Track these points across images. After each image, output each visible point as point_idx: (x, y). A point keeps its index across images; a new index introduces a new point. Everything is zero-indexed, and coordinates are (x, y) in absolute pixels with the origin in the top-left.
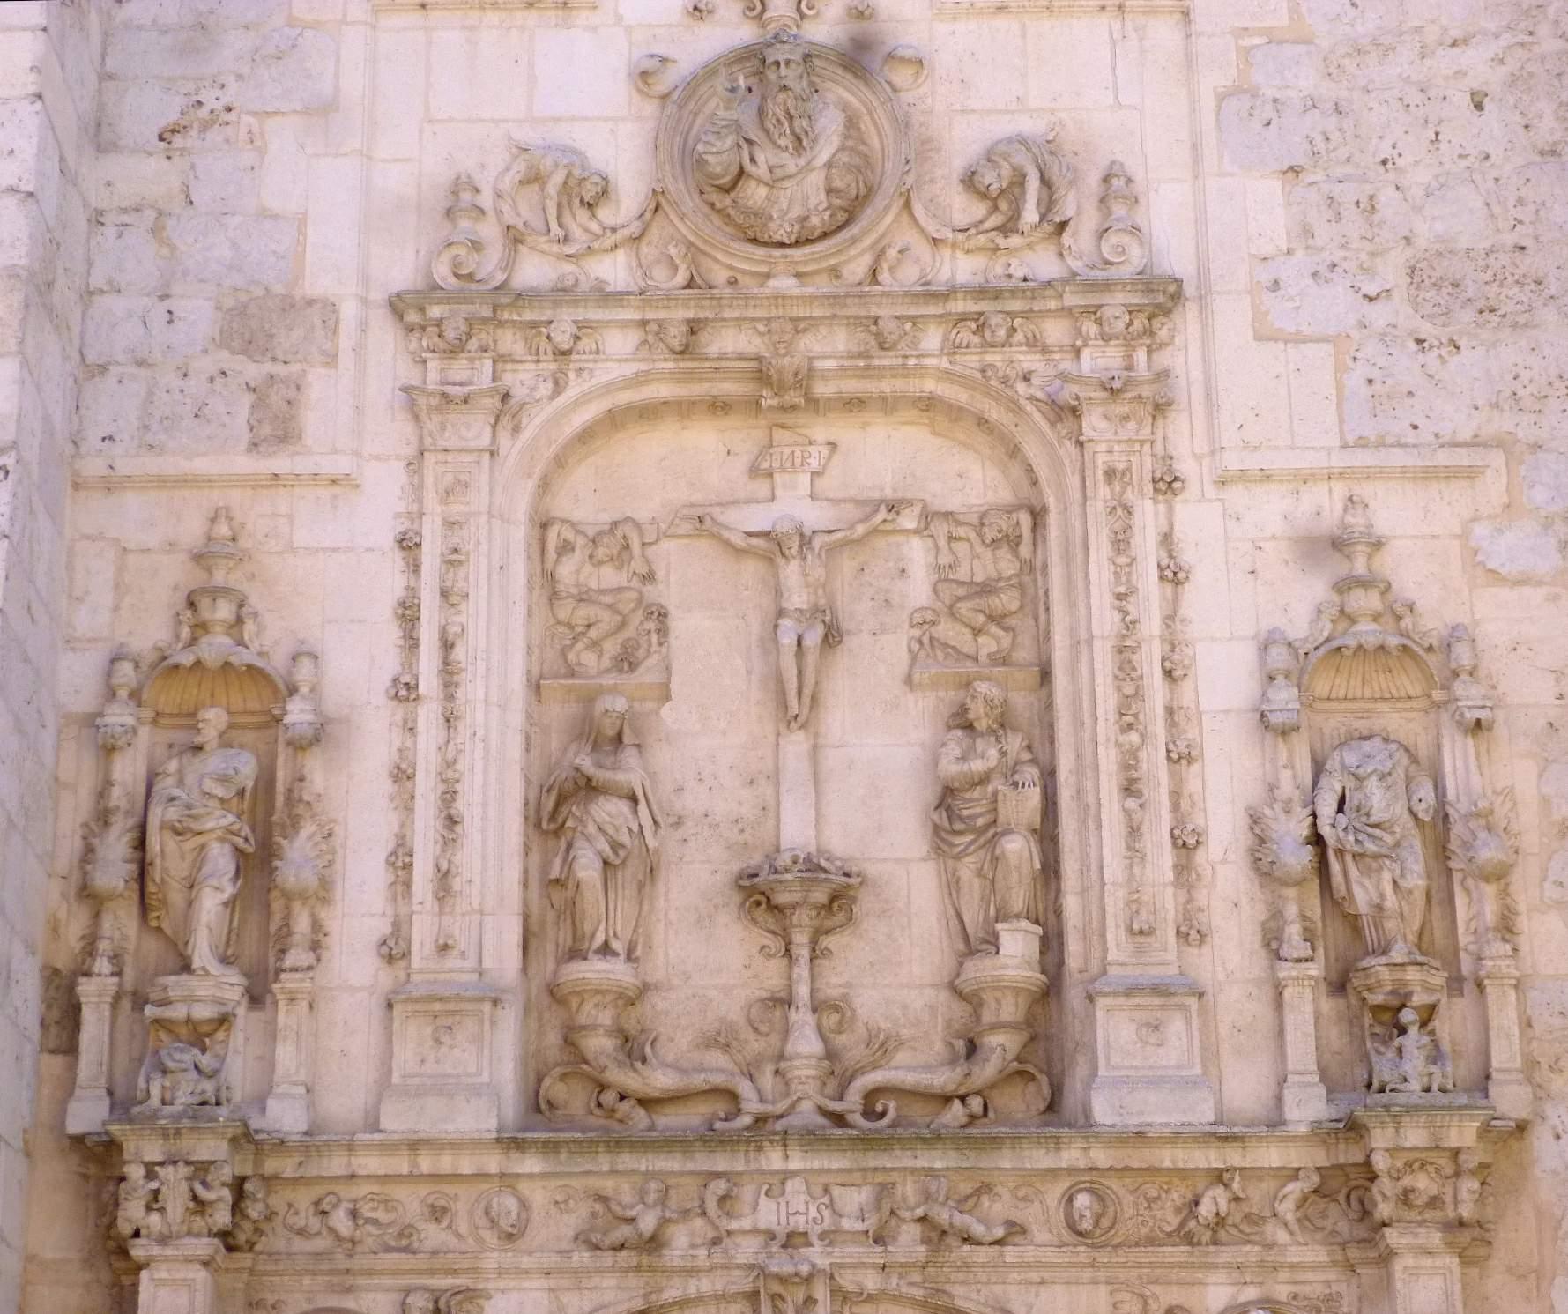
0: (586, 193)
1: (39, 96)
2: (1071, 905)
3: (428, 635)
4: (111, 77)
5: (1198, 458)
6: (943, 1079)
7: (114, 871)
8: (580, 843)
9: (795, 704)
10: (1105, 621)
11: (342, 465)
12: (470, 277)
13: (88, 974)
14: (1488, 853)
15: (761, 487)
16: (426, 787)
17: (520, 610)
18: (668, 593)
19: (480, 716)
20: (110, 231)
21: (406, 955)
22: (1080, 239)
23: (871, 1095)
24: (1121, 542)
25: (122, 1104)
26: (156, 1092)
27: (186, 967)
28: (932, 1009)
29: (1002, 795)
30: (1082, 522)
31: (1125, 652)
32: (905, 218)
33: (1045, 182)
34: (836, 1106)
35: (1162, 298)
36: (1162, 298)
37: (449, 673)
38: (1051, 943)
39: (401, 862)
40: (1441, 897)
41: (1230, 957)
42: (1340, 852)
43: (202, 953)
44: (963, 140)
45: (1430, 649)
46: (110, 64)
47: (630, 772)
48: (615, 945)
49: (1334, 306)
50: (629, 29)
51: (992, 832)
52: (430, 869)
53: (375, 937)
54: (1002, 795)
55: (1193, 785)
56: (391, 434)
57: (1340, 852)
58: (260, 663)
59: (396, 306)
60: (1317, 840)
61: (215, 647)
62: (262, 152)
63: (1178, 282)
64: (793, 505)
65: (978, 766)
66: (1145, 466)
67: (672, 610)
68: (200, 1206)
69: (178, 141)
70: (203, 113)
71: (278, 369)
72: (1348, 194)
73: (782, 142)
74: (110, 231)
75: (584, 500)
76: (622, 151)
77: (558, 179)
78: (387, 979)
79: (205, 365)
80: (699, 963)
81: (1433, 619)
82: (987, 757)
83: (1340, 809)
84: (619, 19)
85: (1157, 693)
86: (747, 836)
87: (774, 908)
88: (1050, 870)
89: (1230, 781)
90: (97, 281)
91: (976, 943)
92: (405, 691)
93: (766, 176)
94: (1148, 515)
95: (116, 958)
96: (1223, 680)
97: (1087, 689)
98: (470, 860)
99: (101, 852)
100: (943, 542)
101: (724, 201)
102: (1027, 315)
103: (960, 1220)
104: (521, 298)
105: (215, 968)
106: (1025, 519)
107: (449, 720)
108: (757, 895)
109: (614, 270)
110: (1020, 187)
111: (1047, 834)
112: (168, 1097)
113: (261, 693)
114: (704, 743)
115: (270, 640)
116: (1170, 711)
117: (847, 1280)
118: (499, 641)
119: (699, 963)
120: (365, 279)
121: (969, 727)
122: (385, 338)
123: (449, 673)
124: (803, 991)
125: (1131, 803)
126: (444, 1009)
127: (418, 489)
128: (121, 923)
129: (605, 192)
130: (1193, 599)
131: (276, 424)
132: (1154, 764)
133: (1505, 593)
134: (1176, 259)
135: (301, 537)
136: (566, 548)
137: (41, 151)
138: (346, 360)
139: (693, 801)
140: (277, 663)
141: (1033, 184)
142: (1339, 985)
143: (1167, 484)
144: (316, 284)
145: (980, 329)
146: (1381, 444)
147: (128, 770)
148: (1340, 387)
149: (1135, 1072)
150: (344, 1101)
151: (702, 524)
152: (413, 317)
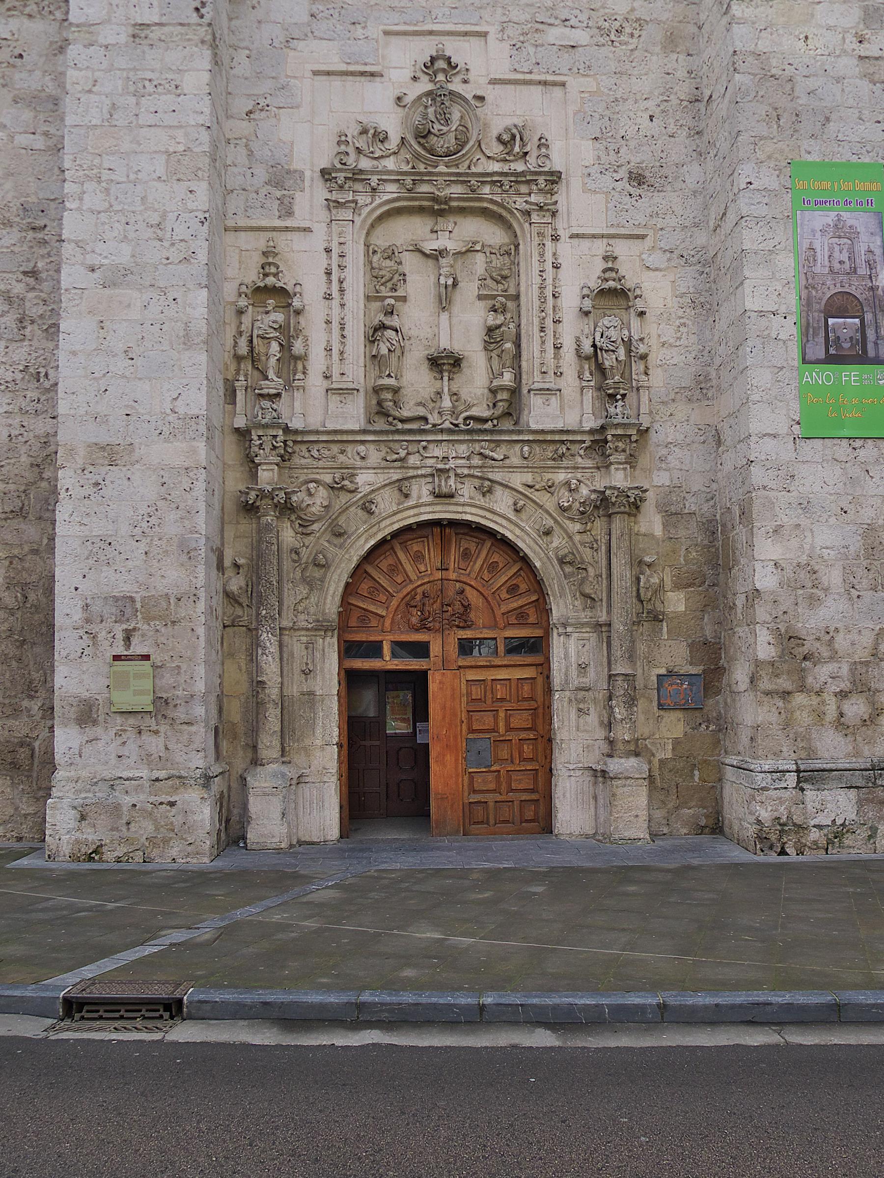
0: (381, 137)
1: (210, 94)
2: (524, 364)
3: (334, 278)
4: (230, 93)
5: (564, 229)
6: (486, 414)
7: (243, 349)
8: (381, 344)
11: (306, 224)
12: (345, 164)
13: (238, 380)
14: (642, 349)
15: (434, 236)
16: (335, 326)
17: (362, 273)
18: (406, 268)
19: (351, 304)
20: (232, 146)
21: (331, 376)
22: (532, 159)
23: (466, 419)
24: (542, 255)
26: (260, 415)
27: (267, 378)
28: (483, 395)
30: (529, 247)
32: (479, 149)
33: (521, 139)
34: (456, 422)
36: (555, 178)
37: (342, 291)
40: (628, 364)
41: (569, 382)
42: (601, 350)
43: (271, 374)
44: (497, 126)
45: (629, 290)
46: (230, 90)
47: (394, 321)
48: (392, 374)
50: (393, 83)
51: (499, 343)
52: (338, 352)
53: (322, 371)
55: (560, 330)
56: (324, 215)
57: (601, 350)
58: (284, 286)
59: (324, 172)
60: (594, 346)
61: (270, 280)
62: (279, 120)
63: (561, 173)
64: (442, 242)
65: (498, 322)
66: (549, 231)
67: (407, 274)
68: (275, 448)
69: (252, 116)
70: (260, 107)
71: (286, 192)
72: (612, 147)
73: (442, 122)
74: (232, 146)
75: (382, 239)
76: (393, 124)
77: (372, 131)
78: (326, 384)
79: (263, 191)
80: (416, 382)
81: (629, 284)
82: (500, 319)
83: (602, 337)
84: (390, 79)
85: (550, 301)
86: (430, 343)
87: (438, 365)
88: (518, 356)
89: (571, 330)
90: (228, 163)
92: (328, 297)
93: (438, 133)
95: (246, 375)
96: (571, 300)
98: (348, 349)
99: (240, 344)
100: (488, 254)
101: (422, 141)
102: (516, 182)
103: (491, 454)
104: (361, 172)
105: (275, 379)
106: (512, 247)
107: (342, 305)
110: (511, 141)
115: (287, 281)
116: (554, 307)
117: (459, 471)
118: (357, 281)
120: (312, 165)
121: (495, 311)
122: (319, 184)
123: (342, 291)
124: (446, 389)
125: (542, 334)
127: (330, 234)
128: (247, 366)
129: (387, 137)
132: (549, 323)
133: (651, 273)
135: (295, 247)
136: (375, 252)
137: (211, 113)
138: (307, 189)
139: (414, 332)
140: (289, 288)
141: (518, 137)
142: (599, 388)
143: (555, 238)
144: (296, 165)
145: (502, 185)
146: (618, 226)
148: (607, 207)
149: (540, 415)
152: (326, 177)
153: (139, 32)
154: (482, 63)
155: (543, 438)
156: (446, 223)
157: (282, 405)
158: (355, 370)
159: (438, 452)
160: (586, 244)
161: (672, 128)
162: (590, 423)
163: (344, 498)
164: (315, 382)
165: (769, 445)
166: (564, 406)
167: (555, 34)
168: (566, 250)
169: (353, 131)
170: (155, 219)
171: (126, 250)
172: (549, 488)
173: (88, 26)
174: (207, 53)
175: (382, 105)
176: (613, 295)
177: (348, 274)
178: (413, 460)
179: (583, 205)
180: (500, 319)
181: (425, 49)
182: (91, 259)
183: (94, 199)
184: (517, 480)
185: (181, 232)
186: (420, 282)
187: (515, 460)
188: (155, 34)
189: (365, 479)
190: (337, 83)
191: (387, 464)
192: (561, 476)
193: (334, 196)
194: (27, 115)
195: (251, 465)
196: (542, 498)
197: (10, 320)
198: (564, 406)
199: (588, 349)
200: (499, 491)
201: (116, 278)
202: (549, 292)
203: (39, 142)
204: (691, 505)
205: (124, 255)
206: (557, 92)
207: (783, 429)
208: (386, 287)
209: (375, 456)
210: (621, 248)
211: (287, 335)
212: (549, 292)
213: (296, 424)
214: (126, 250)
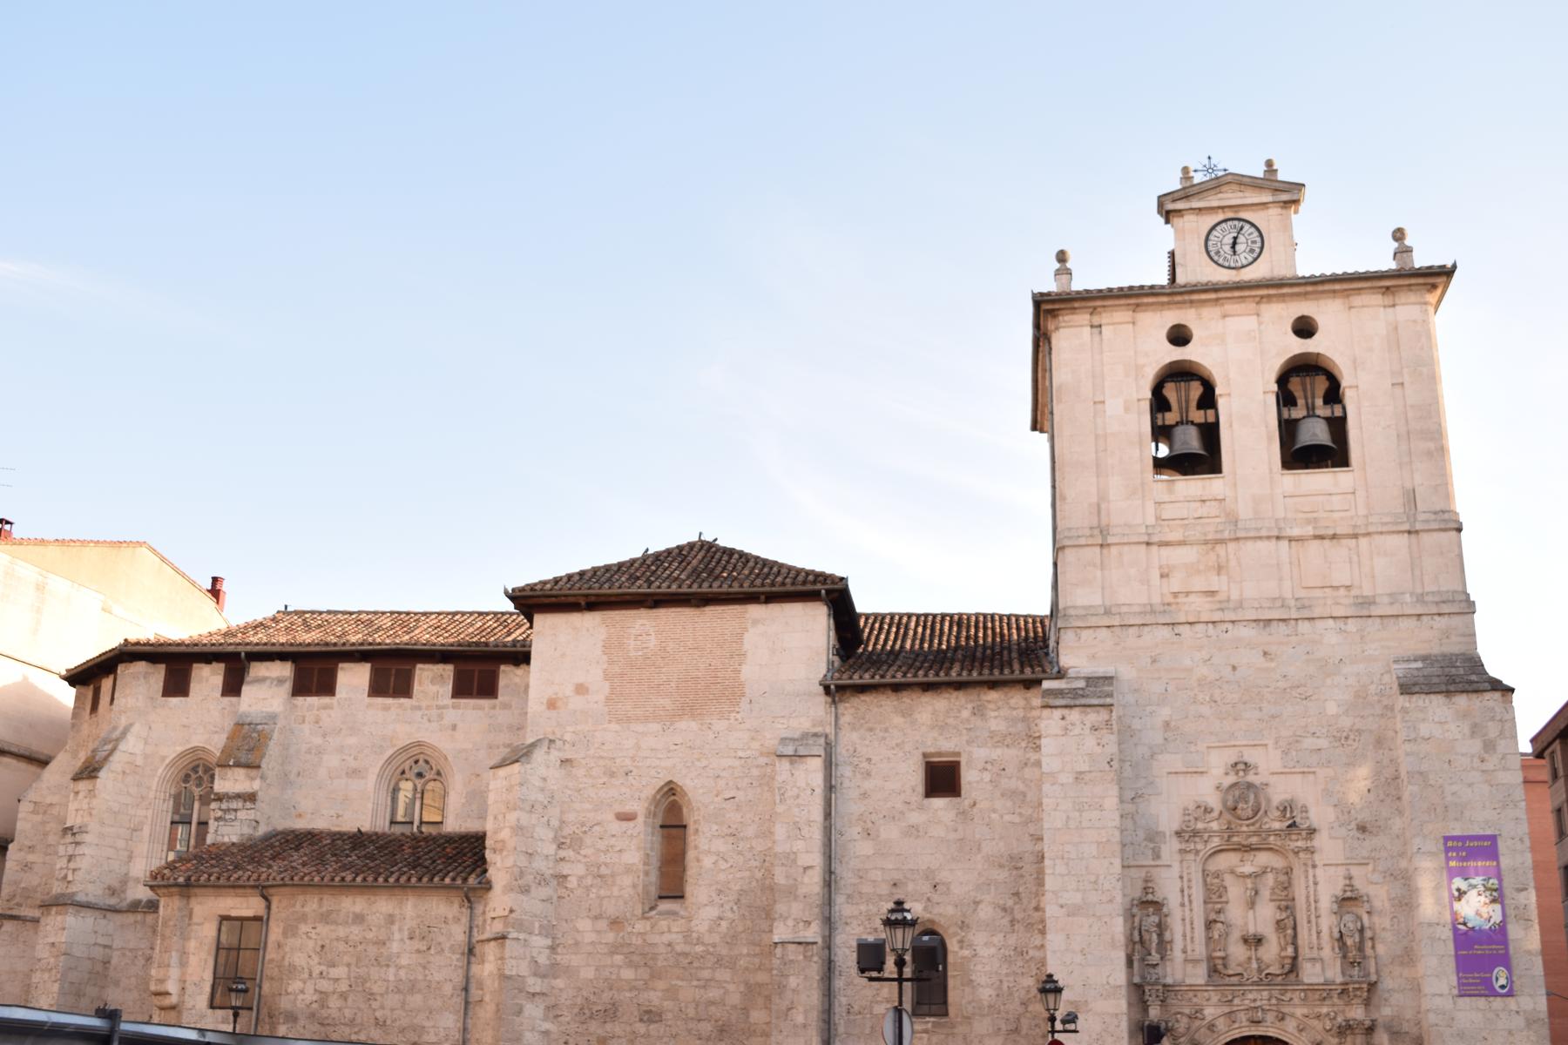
0: (1208, 810)
7: (1137, 938)
9: (1252, 904)
10: (1304, 892)
18: (1227, 883)
25: (1143, 977)
29: (1288, 926)
30: (1298, 873)
31: (1308, 897)
35: (1312, 832)
38: (1296, 950)
39: (1184, 936)
41: (1327, 953)
47: (1222, 918)
49: (1343, 832)
51: (1284, 929)
54: (1288, 926)
56: (1177, 857)
61: (1150, 897)
76: (1214, 801)
80: (1238, 952)
88: (1295, 936)
89: (1327, 922)
91: (1283, 949)
92: (1183, 905)
94: (1311, 871)
96: (1326, 903)
97: (1301, 903)
98: (1196, 935)
108: (1245, 941)
109: (1215, 826)
110: (1286, 808)
111: (1295, 928)
112: (1278, 604)
113: (1157, 905)
114: (1235, 912)
115: (1158, 897)
118: (1198, 893)
119: (1238, 952)
126: (1196, 961)
128: (1138, 947)
130: (1319, 887)
131: (1157, 856)
134: (1315, 825)
143: (1314, 866)
144: (1161, 829)
147: (1137, 920)
149: (1311, 974)
150: (1179, 977)
151: (1232, 872)
153: (1079, 777)
154: (1266, 763)
155: (1312, 989)
156: (1250, 856)
157: (1159, 970)
158: (1200, 950)
159: (1251, 996)
160: (1333, 869)
161: (1382, 796)
162: (1339, 979)
163: (1197, 1023)
164: (1177, 953)
165: (1438, 1001)
166: (1323, 967)
167: (1309, 743)
168: (1319, 872)
169: (1192, 807)
170: (1093, 878)
171: (1079, 896)
172: (1318, 1017)
173: (1052, 774)
174: (1116, 788)
175: (1207, 791)
176: (1348, 900)
177: (1194, 891)
178: (1236, 1001)
179: (1329, 847)
180: (1284, 915)
181: (1231, 756)
182: (1061, 901)
183: (1061, 868)
184: (1299, 1012)
185: (1107, 886)
186: (1235, 892)
187: (1296, 1001)
188: (1087, 777)
189: (1210, 1012)
190: (1181, 778)
191: (1222, 1003)
192: (1325, 1010)
193: (1183, 846)
194: (1009, 804)
195: (1144, 1006)
196: (1315, 1023)
197: (1005, 921)
198: (1323, 967)
199: (1337, 935)
200: (1288, 1019)
201: (1074, 911)
202: (1312, 899)
203: (1017, 819)
204: (1405, 1027)
205: (1076, 898)
206: (1311, 777)
207: (1446, 991)
208: (1214, 894)
209: (1215, 998)
210: (1355, 871)
211: (1161, 928)
212: (1312, 899)
213: (1169, 981)
214: (1079, 896)
